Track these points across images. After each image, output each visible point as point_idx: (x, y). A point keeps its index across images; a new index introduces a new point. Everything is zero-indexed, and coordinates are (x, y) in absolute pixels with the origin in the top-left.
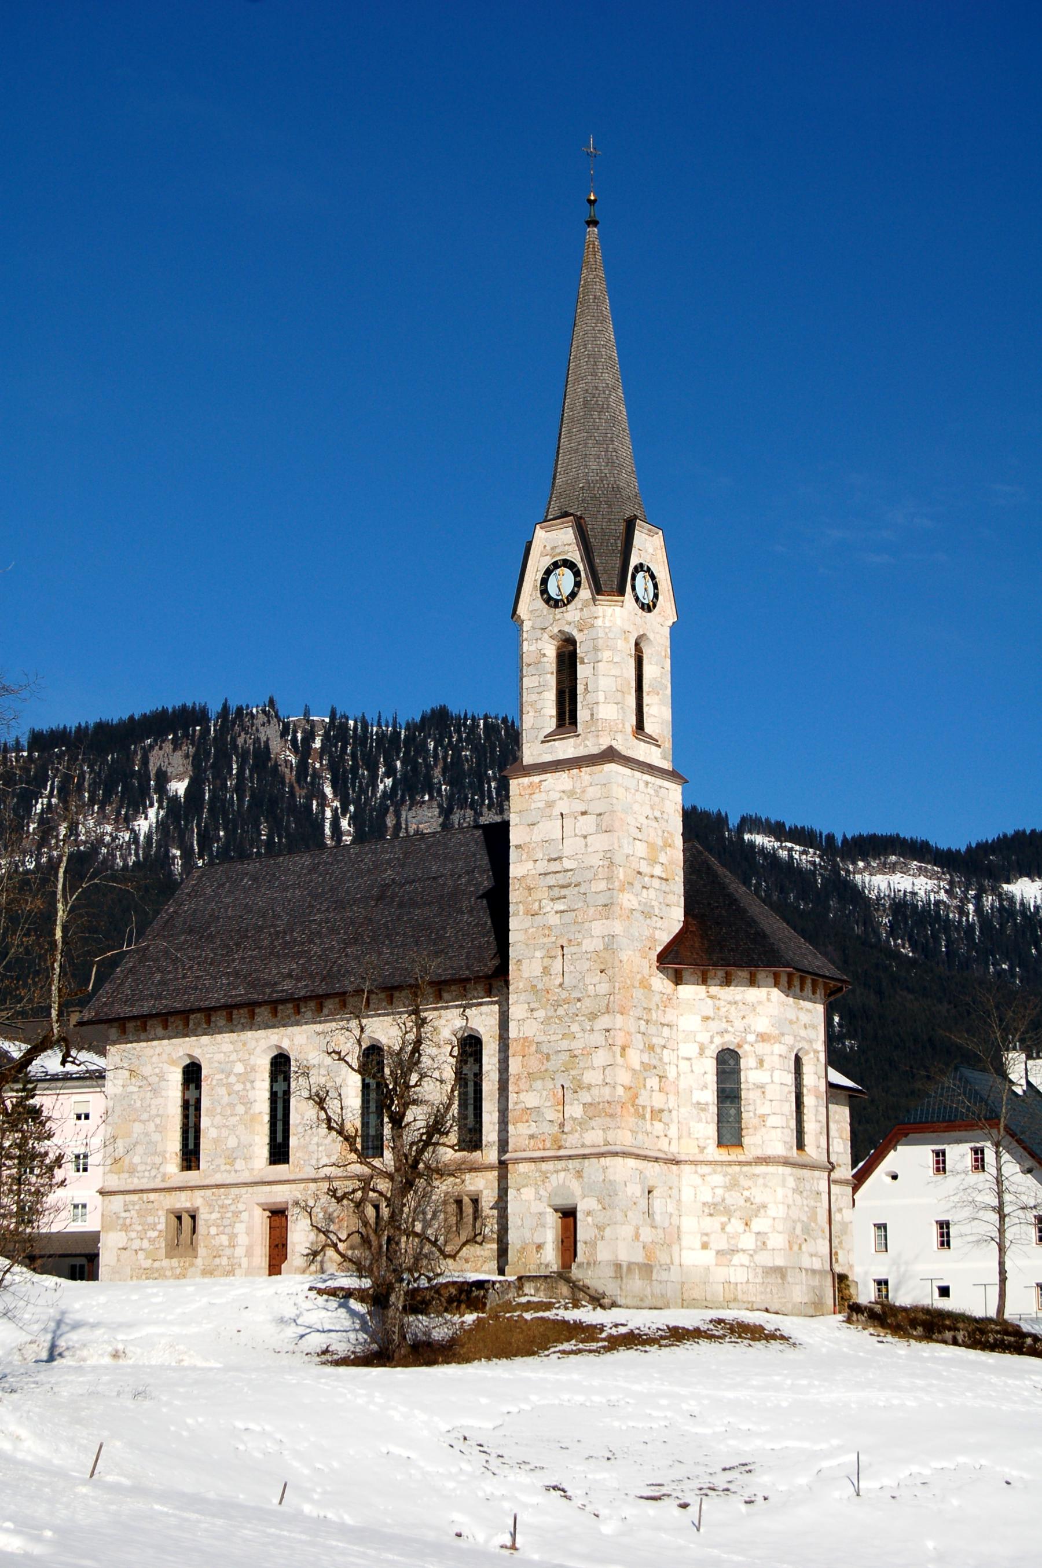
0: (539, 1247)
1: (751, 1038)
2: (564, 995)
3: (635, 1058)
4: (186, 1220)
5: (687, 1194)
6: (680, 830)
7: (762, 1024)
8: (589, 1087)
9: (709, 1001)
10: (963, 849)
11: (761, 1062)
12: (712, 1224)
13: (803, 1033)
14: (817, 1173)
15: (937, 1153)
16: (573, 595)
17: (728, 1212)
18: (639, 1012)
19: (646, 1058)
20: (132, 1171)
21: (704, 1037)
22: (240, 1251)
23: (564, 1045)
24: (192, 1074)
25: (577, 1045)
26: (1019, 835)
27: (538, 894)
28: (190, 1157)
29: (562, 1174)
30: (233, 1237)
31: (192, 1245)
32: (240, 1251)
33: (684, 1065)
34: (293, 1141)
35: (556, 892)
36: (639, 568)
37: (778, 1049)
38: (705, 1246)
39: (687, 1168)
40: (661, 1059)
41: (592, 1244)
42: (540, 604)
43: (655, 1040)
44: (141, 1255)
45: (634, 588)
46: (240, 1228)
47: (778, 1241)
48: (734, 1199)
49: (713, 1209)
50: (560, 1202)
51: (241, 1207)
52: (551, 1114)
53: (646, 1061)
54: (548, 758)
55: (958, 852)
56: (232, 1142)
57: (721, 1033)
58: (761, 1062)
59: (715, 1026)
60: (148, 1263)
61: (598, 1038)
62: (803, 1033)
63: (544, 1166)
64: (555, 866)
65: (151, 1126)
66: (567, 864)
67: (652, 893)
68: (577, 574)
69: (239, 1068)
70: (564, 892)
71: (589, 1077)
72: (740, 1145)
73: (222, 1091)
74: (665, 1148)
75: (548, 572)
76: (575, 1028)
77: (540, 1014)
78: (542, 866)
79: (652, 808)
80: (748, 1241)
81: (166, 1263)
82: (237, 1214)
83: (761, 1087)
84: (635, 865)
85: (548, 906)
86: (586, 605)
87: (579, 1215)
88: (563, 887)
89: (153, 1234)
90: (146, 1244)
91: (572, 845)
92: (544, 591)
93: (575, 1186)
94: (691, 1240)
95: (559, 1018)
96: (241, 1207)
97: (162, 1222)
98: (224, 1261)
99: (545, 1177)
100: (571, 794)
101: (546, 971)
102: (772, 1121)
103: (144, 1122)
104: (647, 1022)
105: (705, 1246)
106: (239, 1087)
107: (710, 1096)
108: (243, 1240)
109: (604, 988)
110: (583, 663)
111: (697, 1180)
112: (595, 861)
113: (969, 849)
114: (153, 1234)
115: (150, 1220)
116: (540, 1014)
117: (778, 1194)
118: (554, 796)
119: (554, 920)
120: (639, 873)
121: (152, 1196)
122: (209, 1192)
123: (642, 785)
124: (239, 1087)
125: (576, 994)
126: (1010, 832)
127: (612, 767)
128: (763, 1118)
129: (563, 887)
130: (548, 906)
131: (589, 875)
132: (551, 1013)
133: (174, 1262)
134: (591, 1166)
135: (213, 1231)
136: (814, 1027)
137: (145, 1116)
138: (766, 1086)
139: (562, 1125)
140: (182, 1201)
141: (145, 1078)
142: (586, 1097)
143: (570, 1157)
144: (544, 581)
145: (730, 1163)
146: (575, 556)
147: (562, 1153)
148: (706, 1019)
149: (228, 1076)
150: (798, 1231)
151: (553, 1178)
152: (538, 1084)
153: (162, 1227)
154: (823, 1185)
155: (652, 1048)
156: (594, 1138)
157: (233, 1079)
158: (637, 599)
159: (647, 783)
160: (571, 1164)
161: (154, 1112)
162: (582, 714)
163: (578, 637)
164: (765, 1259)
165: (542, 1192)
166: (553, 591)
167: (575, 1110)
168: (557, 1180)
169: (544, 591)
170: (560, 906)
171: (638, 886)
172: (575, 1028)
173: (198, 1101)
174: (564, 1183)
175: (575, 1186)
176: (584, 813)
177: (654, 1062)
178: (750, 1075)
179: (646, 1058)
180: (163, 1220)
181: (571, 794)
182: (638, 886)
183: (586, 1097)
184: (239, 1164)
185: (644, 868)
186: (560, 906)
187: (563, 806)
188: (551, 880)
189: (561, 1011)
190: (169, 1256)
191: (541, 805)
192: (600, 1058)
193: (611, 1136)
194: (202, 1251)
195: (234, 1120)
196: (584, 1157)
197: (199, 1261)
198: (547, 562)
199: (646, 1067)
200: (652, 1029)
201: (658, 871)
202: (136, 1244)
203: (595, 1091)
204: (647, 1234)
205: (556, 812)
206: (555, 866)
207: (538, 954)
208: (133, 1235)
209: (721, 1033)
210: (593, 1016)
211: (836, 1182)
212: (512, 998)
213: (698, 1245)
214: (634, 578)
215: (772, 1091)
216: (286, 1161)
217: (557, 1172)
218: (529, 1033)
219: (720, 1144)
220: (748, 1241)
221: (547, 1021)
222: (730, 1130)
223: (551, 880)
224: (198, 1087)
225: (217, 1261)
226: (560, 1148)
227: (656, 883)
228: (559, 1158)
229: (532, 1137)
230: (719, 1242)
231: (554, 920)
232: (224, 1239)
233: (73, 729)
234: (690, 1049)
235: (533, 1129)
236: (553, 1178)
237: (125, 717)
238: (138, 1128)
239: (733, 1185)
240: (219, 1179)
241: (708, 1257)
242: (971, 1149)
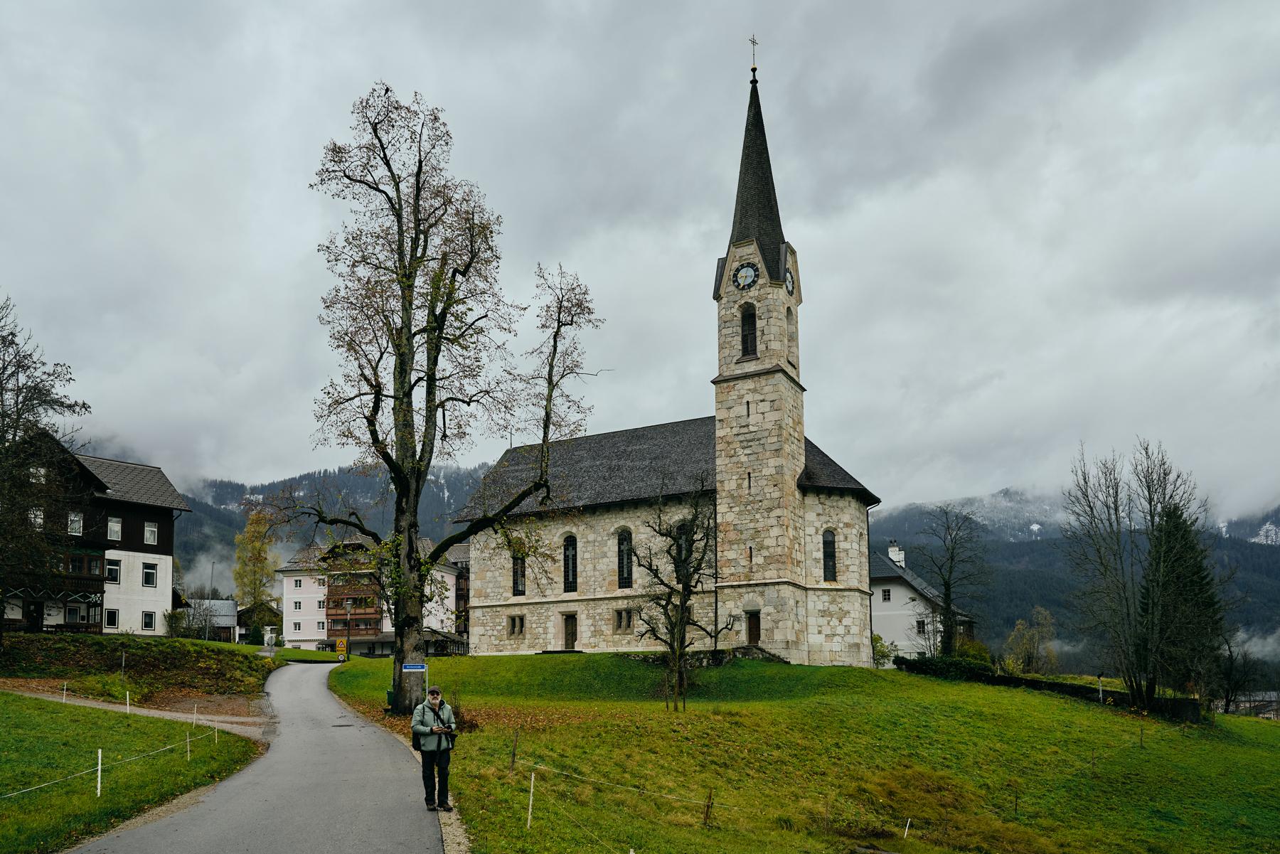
0: (738, 632)
1: (841, 525)
3: (791, 532)
4: (517, 621)
5: (811, 605)
7: (846, 518)
11: (846, 538)
12: (823, 621)
15: (884, 591)
16: (754, 282)
17: (831, 615)
20: (487, 597)
21: (818, 524)
22: (550, 636)
23: (752, 525)
25: (759, 526)
27: (734, 446)
33: (808, 538)
34: (579, 580)
35: (745, 444)
37: (854, 531)
38: (820, 632)
39: (810, 593)
41: (771, 631)
42: (732, 288)
46: (550, 624)
47: (855, 630)
48: (833, 608)
49: (824, 613)
50: (749, 608)
52: (744, 562)
54: (739, 372)
57: (827, 522)
58: (846, 538)
59: (823, 518)
61: (773, 521)
63: (741, 590)
66: (752, 429)
68: (756, 270)
71: (767, 542)
72: (835, 580)
75: (738, 270)
76: (758, 516)
77: (737, 509)
78: (735, 431)
80: (840, 630)
82: (548, 617)
83: (846, 551)
85: (740, 452)
86: (762, 286)
91: (752, 419)
93: (760, 601)
94: (813, 629)
97: (505, 622)
99: (741, 595)
101: (739, 486)
102: (851, 568)
105: (820, 632)
107: (820, 555)
108: (551, 630)
109: (776, 495)
110: (578, 426)
112: (769, 426)
117: (854, 605)
118: (742, 392)
119: (744, 459)
125: (758, 498)
127: (780, 375)
128: (848, 566)
130: (740, 452)
131: (766, 434)
132: (743, 508)
134: (770, 591)
140: (516, 611)
142: (765, 553)
143: (757, 585)
144: (735, 276)
145: (832, 590)
146: (757, 259)
148: (818, 515)
152: (735, 547)
156: (771, 575)
160: (757, 589)
162: (760, 347)
163: (757, 305)
164: (849, 639)
167: (758, 560)
172: (758, 516)
174: (752, 599)
175: (760, 601)
178: (841, 545)
181: (754, 391)
183: (765, 553)
186: (748, 451)
188: (741, 438)
189: (749, 508)
190: (614, 634)
192: (775, 532)
193: (781, 573)
194: (528, 636)
196: (766, 584)
198: (736, 265)
199: (795, 538)
202: (490, 633)
203: (772, 550)
204: (797, 626)
205: (744, 401)
206: (745, 430)
209: (827, 522)
210: (770, 510)
212: (719, 501)
215: (853, 553)
216: (575, 590)
218: (729, 520)
219: (825, 580)
220: (840, 630)
221: (740, 513)
222: (831, 572)
223: (741, 438)
228: (750, 585)
230: (827, 631)
231: (744, 459)
232: (541, 630)
234: (810, 530)
241: (822, 638)
242: (562, 614)
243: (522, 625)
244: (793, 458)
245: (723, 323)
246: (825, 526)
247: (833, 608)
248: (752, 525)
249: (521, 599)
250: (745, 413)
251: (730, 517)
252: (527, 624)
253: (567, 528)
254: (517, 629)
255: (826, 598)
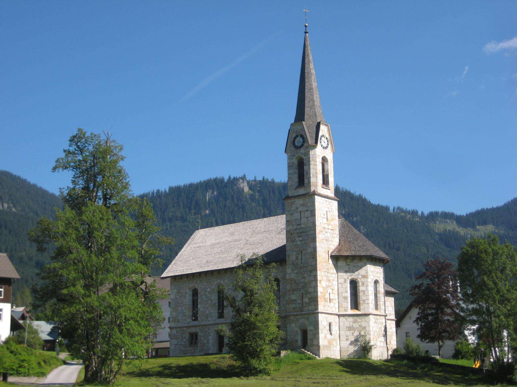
0: (297, 341)
1: (360, 277)
2: (302, 265)
6: (337, 215)
8: (310, 293)
9: (347, 266)
10: (465, 215)
13: (376, 275)
14: (382, 317)
18: (325, 270)
19: (327, 284)
20: (178, 322)
22: (210, 345)
23: (303, 280)
24: (195, 293)
25: (306, 280)
26: (483, 210)
28: (196, 319)
29: (303, 319)
30: (208, 340)
31: (196, 343)
32: (210, 345)
36: (323, 136)
38: (347, 340)
40: (332, 284)
42: (293, 148)
43: (330, 278)
44: (182, 346)
45: (321, 142)
48: (356, 325)
51: (210, 331)
52: (299, 301)
53: (328, 284)
54: (296, 194)
55: (463, 216)
56: (207, 312)
60: (183, 349)
62: (376, 275)
64: (299, 227)
65: (183, 308)
66: (302, 226)
67: (329, 234)
69: (209, 290)
70: (302, 234)
73: (204, 297)
74: (334, 310)
75: (295, 138)
77: (296, 271)
78: (295, 227)
79: (328, 208)
81: (189, 348)
84: (323, 225)
85: (297, 239)
87: (308, 331)
88: (301, 233)
89: (185, 340)
90: (183, 343)
91: (303, 220)
92: (294, 144)
95: (301, 272)
96: (210, 331)
98: (206, 348)
99: (298, 320)
100: (303, 205)
101: (297, 258)
103: (181, 307)
104: (328, 273)
105: (347, 340)
106: (209, 296)
108: (211, 341)
111: (345, 320)
113: (467, 215)
114: (185, 340)
115: (184, 336)
116: (296, 271)
118: (298, 206)
120: (324, 228)
121: (184, 329)
122: (201, 327)
123: (325, 201)
124: (209, 296)
125: (306, 265)
126: (480, 209)
129: (301, 233)
130: (297, 239)
133: (191, 348)
135: (202, 339)
136: (380, 273)
137: (182, 305)
138: (367, 292)
139: (303, 304)
140: (193, 330)
141: (181, 293)
142: (309, 296)
143: (305, 314)
144: (294, 141)
147: (303, 313)
149: (206, 292)
150: (376, 334)
151: (300, 320)
152: (295, 292)
153: (187, 338)
154: (384, 321)
155: (329, 281)
157: (207, 293)
158: (322, 146)
159: (326, 201)
161: (184, 303)
165: (297, 325)
166: (296, 144)
168: (302, 321)
169: (294, 144)
170: (301, 239)
171: (324, 232)
172: (306, 275)
173: (197, 300)
175: (307, 323)
176: (307, 211)
177: (330, 285)
179: (327, 284)
180: (188, 336)
181: (303, 205)
182: (324, 232)
183: (309, 296)
184: (210, 319)
185: (326, 226)
186: (301, 239)
187: (301, 209)
188: (298, 231)
189: (301, 270)
191: (294, 208)
194: (199, 345)
195: (207, 305)
197: (199, 348)
198: (294, 135)
200: (329, 275)
201: (330, 227)
202: (180, 343)
206: (299, 227)
207: (295, 253)
208: (179, 340)
211: (388, 319)
213: (345, 339)
214: (321, 139)
217: (301, 318)
219: (351, 309)
221: (297, 273)
223: (298, 231)
224: (197, 296)
225: (204, 348)
226: (302, 311)
227: (330, 231)
228: (302, 314)
229: (294, 308)
231: (299, 243)
232: (205, 341)
233: (155, 192)
235: (294, 306)
236: (300, 320)
237: (199, 181)
238: (180, 308)
239: (355, 322)
240: (203, 323)
243: (196, 338)
244: (326, 240)
245: (290, 167)
246: (350, 278)
247: (356, 325)
248: (303, 280)
249: (195, 323)
250: (299, 217)
251: (293, 276)
252: (199, 338)
253: (219, 281)
254: (194, 341)
255: (351, 319)
